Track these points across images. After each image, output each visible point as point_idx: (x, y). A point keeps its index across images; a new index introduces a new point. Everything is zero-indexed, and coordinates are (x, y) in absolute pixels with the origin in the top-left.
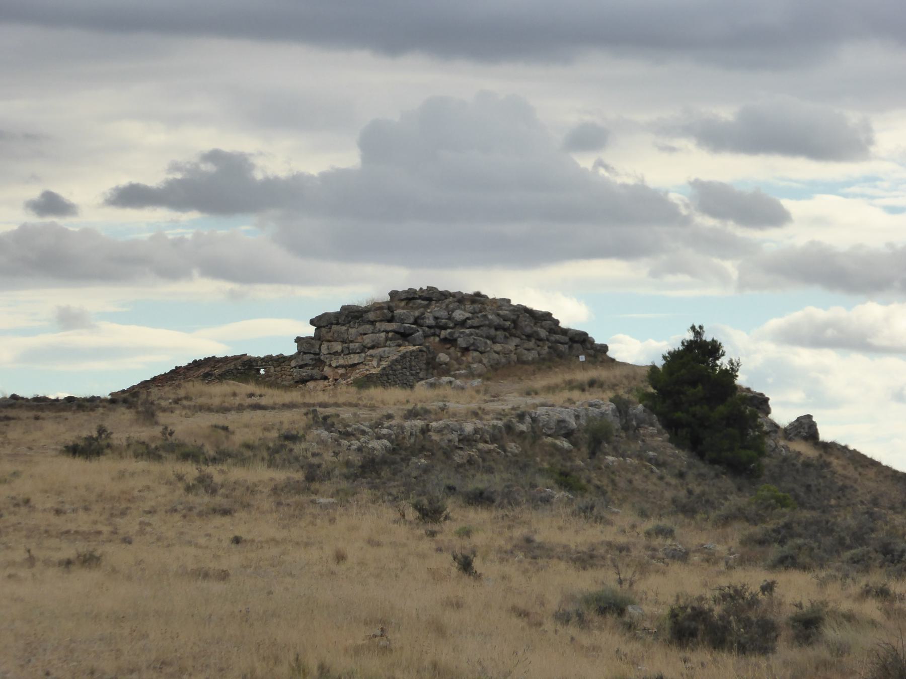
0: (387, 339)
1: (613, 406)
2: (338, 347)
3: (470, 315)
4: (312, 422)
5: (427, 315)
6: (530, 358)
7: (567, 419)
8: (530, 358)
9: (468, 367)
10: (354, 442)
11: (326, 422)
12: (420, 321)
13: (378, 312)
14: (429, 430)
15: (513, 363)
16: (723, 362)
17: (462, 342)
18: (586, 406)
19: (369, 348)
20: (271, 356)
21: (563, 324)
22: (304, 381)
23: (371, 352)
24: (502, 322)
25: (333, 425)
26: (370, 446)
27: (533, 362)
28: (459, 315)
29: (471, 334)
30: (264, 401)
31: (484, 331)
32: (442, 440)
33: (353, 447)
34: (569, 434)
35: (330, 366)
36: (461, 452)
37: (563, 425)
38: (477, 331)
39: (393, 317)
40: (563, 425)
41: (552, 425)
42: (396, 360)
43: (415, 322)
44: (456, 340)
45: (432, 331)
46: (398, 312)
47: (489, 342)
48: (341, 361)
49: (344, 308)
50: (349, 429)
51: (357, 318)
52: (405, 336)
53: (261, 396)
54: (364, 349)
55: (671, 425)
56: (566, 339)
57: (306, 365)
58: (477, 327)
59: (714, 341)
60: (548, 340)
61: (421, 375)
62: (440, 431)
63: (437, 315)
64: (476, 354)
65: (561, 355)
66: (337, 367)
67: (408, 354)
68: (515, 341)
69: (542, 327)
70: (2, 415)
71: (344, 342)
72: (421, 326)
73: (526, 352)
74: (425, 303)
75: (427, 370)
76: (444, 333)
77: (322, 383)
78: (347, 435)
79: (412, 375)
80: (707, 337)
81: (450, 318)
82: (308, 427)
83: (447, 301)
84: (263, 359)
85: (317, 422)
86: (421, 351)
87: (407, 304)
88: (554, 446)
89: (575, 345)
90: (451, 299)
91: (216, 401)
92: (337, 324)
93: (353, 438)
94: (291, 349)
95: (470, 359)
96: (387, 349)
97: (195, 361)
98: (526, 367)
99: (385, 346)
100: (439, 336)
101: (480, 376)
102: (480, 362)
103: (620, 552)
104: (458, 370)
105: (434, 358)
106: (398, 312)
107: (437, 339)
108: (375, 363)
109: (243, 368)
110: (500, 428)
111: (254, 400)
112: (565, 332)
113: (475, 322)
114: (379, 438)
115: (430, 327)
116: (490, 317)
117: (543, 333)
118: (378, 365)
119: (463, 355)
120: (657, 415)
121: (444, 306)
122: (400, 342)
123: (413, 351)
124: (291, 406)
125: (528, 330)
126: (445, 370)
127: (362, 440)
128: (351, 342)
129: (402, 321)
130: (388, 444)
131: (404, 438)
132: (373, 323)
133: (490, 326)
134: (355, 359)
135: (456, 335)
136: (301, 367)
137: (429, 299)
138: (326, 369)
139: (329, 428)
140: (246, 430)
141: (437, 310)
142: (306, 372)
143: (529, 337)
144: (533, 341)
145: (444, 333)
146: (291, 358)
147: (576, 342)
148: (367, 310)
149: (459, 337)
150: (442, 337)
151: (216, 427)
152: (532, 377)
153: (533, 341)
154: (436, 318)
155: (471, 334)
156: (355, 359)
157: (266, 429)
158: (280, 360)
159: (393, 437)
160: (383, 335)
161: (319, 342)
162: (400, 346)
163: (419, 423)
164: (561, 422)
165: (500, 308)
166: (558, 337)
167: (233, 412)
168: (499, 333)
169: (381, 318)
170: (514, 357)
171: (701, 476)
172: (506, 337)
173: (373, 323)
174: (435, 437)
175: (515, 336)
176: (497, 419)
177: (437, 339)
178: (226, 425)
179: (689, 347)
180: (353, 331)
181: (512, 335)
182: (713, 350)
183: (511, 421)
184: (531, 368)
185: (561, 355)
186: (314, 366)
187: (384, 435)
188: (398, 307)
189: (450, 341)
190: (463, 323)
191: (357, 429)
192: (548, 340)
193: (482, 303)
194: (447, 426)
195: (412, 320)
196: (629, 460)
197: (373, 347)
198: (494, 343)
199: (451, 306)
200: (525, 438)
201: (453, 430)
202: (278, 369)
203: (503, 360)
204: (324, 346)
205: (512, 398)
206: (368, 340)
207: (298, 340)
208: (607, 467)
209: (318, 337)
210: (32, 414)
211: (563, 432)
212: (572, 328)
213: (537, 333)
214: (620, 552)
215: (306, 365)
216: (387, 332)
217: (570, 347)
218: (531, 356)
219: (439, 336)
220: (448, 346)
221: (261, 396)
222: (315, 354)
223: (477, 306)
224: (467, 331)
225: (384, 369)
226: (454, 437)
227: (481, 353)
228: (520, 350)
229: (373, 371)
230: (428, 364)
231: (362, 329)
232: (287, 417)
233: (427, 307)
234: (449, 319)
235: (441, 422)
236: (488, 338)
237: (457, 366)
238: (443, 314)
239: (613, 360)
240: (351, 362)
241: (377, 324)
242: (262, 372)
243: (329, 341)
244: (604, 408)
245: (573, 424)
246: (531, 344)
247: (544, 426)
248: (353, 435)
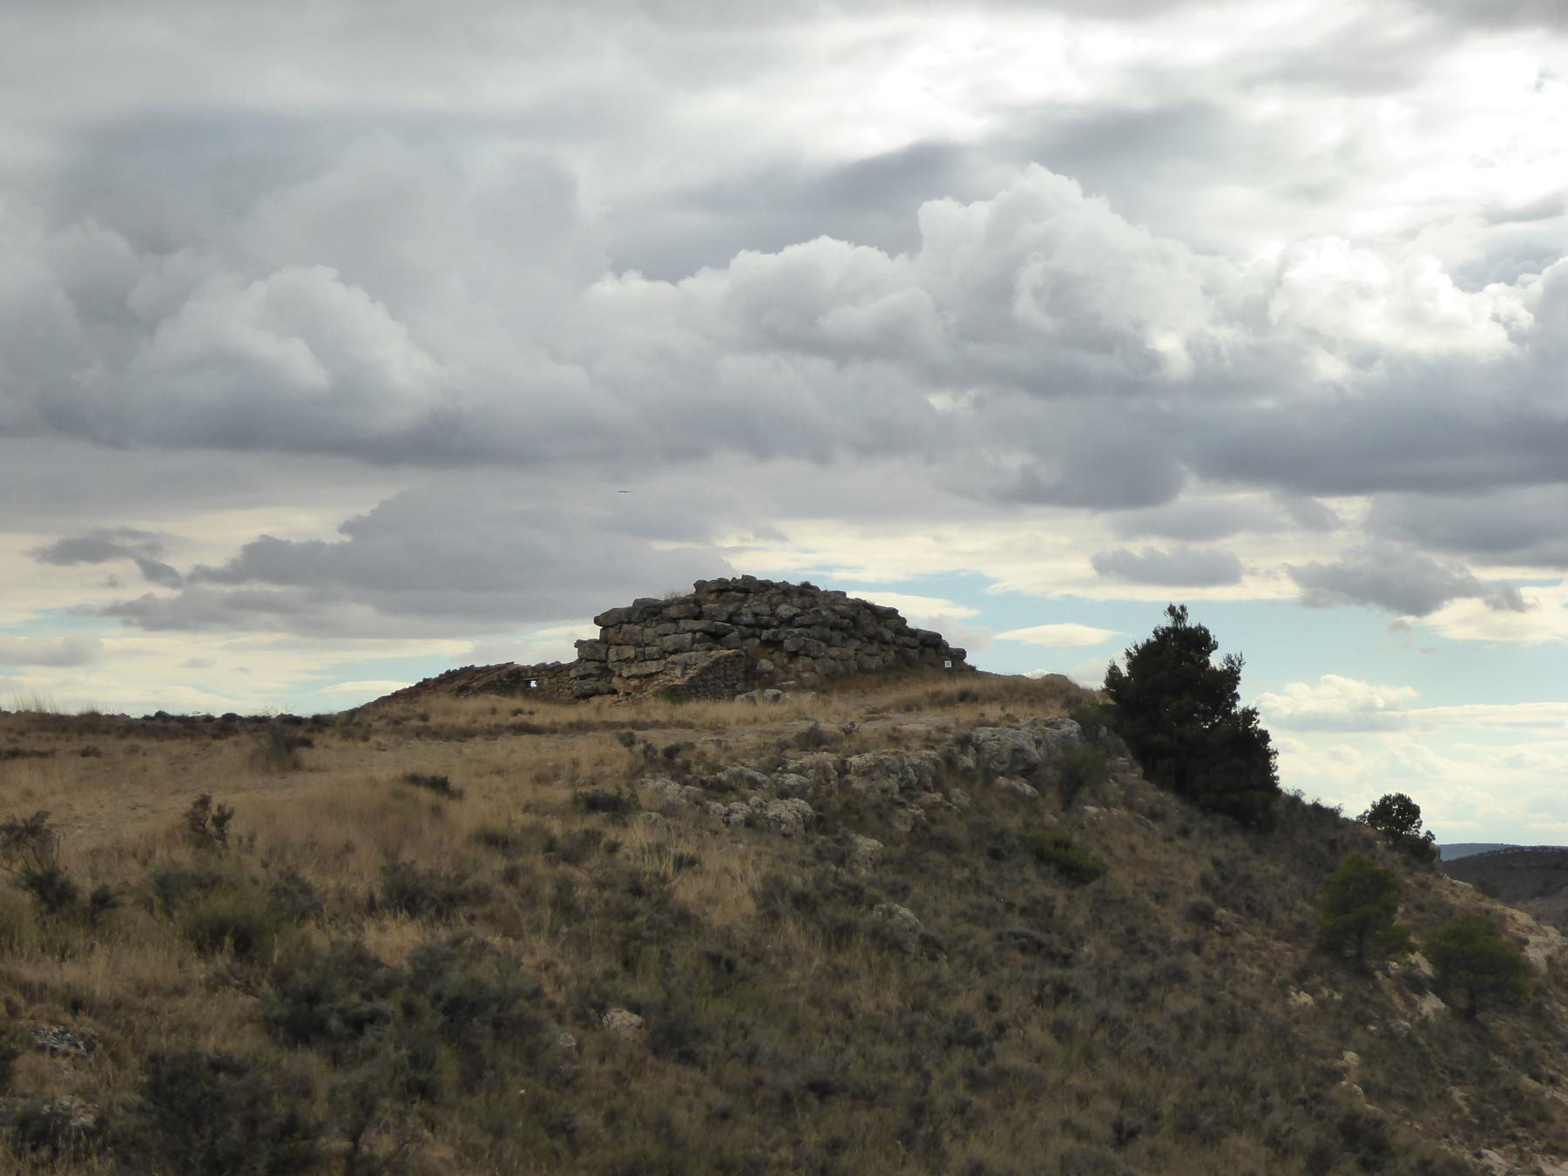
0: (694, 641)
1: (1076, 726)
2: (630, 652)
4: (642, 762)
5: (744, 610)
7: (1027, 747)
9: (798, 677)
10: (735, 805)
11: (671, 761)
12: (736, 619)
14: (847, 772)
16: (1216, 661)
17: (789, 645)
18: (1041, 726)
20: (544, 665)
21: (910, 625)
22: (586, 696)
23: (673, 658)
25: (687, 767)
26: (771, 814)
27: (877, 671)
28: (784, 610)
30: (536, 720)
32: (870, 789)
33: (735, 817)
34: (1030, 771)
36: (901, 811)
37: (1020, 756)
40: (1020, 756)
41: (1006, 755)
42: (707, 668)
43: (729, 620)
46: (707, 606)
48: (634, 671)
50: (723, 776)
51: (655, 614)
52: (716, 637)
53: (531, 713)
54: (664, 654)
55: (1148, 757)
56: (916, 642)
57: (589, 675)
58: (808, 626)
59: (1200, 628)
61: (738, 687)
62: (865, 773)
63: (757, 610)
64: (808, 660)
65: (910, 663)
68: (856, 644)
71: (638, 645)
72: (737, 624)
74: (741, 595)
75: (746, 680)
76: (766, 634)
77: (610, 699)
78: (720, 789)
80: (1191, 622)
81: (772, 615)
82: (635, 773)
83: (769, 593)
84: (534, 669)
85: (652, 761)
86: (738, 656)
88: (1013, 791)
90: (774, 591)
91: (462, 721)
92: (629, 622)
93: (734, 797)
94: (570, 656)
95: (800, 666)
97: (448, 672)
101: (813, 688)
102: (813, 670)
105: (754, 666)
106: (707, 606)
108: (678, 672)
109: (509, 679)
110: (936, 763)
111: (521, 718)
112: (914, 633)
113: (806, 619)
114: (784, 795)
115: (747, 626)
117: (889, 635)
118: (683, 675)
119: (790, 661)
120: (1125, 738)
122: (710, 644)
123: (728, 656)
124: (580, 727)
125: (871, 630)
126: (767, 681)
127: (753, 800)
129: (713, 618)
130: (808, 808)
131: (830, 793)
132: (675, 620)
133: (824, 625)
134: (653, 667)
135: (782, 636)
136: (583, 678)
137: (746, 591)
138: (615, 680)
139: (681, 774)
140: (497, 780)
142: (588, 685)
143: (871, 639)
145: (766, 634)
146: (570, 666)
147: (928, 646)
148: (668, 604)
151: (415, 780)
154: (755, 615)
155: (801, 635)
156: (653, 667)
157: (543, 779)
158: (556, 670)
159: (810, 791)
162: (710, 649)
163: (828, 758)
164: (1018, 751)
165: (834, 602)
166: (906, 639)
167: (478, 739)
170: (853, 664)
171: (1209, 833)
172: (844, 639)
173: (675, 620)
174: (859, 784)
176: (927, 747)
178: (441, 774)
179: (1163, 637)
180: (648, 631)
181: (852, 636)
182: (1200, 641)
183: (950, 751)
186: (600, 677)
187: (792, 787)
188: (706, 601)
189: (774, 644)
190: (789, 621)
191: (740, 775)
193: (813, 596)
194: (880, 764)
195: (725, 617)
196: (1115, 812)
197: (675, 652)
198: (829, 646)
199: (774, 600)
200: (973, 781)
201: (889, 771)
203: (841, 668)
204: (613, 651)
206: (669, 642)
207: (579, 644)
208: (1093, 824)
209: (604, 639)
210: (79, 744)
211: (1020, 768)
212: (922, 628)
213: (881, 635)
215: (589, 675)
216: (694, 632)
217: (921, 652)
218: (874, 663)
221: (531, 713)
223: (807, 600)
224: (796, 631)
225: (691, 679)
226: (893, 783)
228: (860, 655)
229: (677, 682)
230: (746, 673)
231: (661, 629)
232: (585, 749)
233: (743, 600)
235: (868, 756)
237: (783, 676)
238: (765, 609)
239: (973, 669)
240: (646, 671)
242: (533, 684)
244: (1065, 729)
245: (1036, 754)
246: (874, 648)
247: (992, 758)
248: (733, 789)
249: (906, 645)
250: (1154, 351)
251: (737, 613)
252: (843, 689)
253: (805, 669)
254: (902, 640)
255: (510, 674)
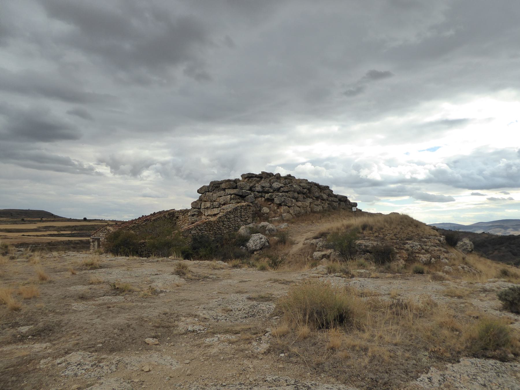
0: (231, 199)
2: (208, 204)
3: (283, 185)
5: (257, 185)
6: (318, 210)
8: (318, 210)
13: (227, 183)
15: (308, 212)
17: (277, 201)
24: (302, 190)
27: (319, 212)
28: (276, 185)
29: (283, 196)
31: (290, 194)
38: (286, 194)
39: (236, 186)
42: (230, 212)
44: (273, 199)
45: (260, 194)
47: (293, 200)
49: (211, 183)
51: (217, 187)
52: (243, 197)
54: (220, 205)
56: (337, 200)
58: (287, 192)
60: (327, 200)
61: (248, 221)
63: (264, 185)
65: (334, 209)
66: (207, 216)
67: (239, 208)
68: (310, 200)
69: (324, 193)
70: (519, 195)
73: (316, 206)
76: (267, 196)
79: (242, 221)
83: (270, 178)
86: (249, 205)
87: (248, 180)
89: (341, 203)
92: (209, 191)
95: (282, 211)
96: (231, 205)
98: (316, 214)
100: (264, 197)
101: (287, 221)
102: (289, 212)
104: (274, 217)
105: (260, 210)
107: (263, 199)
112: (336, 196)
113: (286, 189)
115: (258, 192)
116: (294, 186)
117: (325, 196)
119: (278, 208)
121: (268, 180)
125: (317, 194)
128: (215, 201)
129: (242, 188)
133: (294, 191)
141: (265, 183)
143: (317, 198)
144: (320, 200)
145: (267, 196)
147: (342, 201)
149: (275, 197)
150: (266, 198)
152: (320, 221)
153: (320, 200)
154: (263, 187)
158: (187, 211)
161: (200, 202)
166: (332, 198)
168: (300, 195)
169: (229, 186)
170: (309, 209)
172: (304, 198)
173: (224, 189)
175: (309, 198)
177: (263, 199)
180: (215, 195)
181: (308, 197)
184: (318, 216)
185: (334, 209)
189: (271, 200)
190: (278, 190)
192: (327, 200)
195: (248, 188)
197: (224, 204)
198: (297, 201)
199: (272, 180)
202: (183, 217)
203: (303, 211)
204: (203, 204)
205: (346, 222)
206: (222, 200)
209: (200, 200)
213: (321, 196)
215: (195, 215)
216: (231, 195)
217: (339, 204)
219: (264, 197)
220: (269, 203)
222: (199, 209)
224: (280, 194)
225: (220, 218)
227: (289, 207)
231: (218, 194)
234: (271, 187)
236: (293, 198)
237: (273, 215)
238: (268, 185)
241: (226, 190)
243: (205, 201)
246: (319, 202)
249: (333, 201)
250: (362, 178)
251: (254, 186)
252: (303, 221)
253: (284, 212)
254: (330, 199)
255: (169, 214)
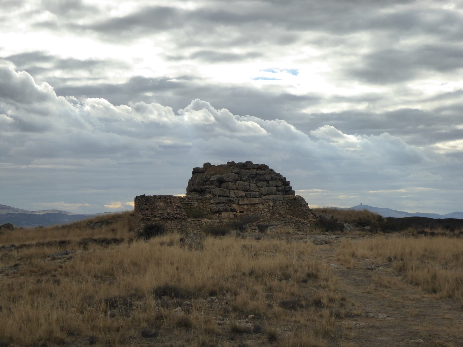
2: (243, 194)
19: (265, 195)
35: (238, 204)
48: (246, 202)
54: (261, 195)
99: (276, 194)
103: (85, 248)
128: (252, 191)
132: (267, 181)
142: (221, 207)
160: (275, 188)
195: (125, 306)
202: (201, 204)
206: (264, 190)
214: (85, 248)
240: (253, 202)
